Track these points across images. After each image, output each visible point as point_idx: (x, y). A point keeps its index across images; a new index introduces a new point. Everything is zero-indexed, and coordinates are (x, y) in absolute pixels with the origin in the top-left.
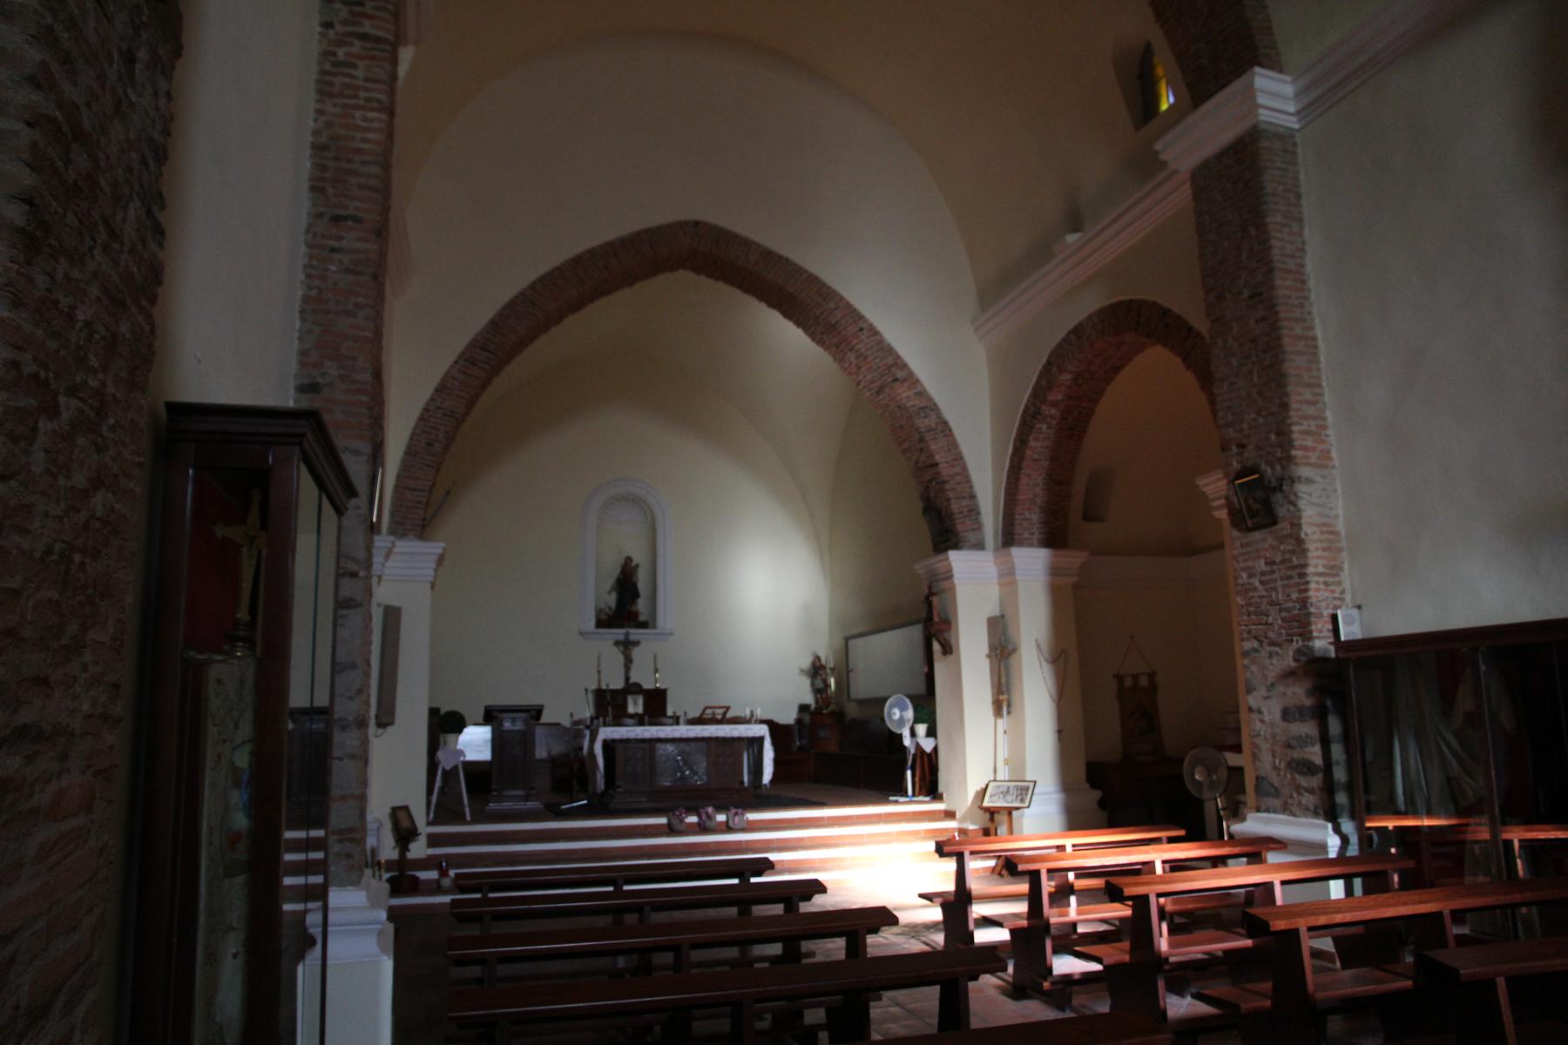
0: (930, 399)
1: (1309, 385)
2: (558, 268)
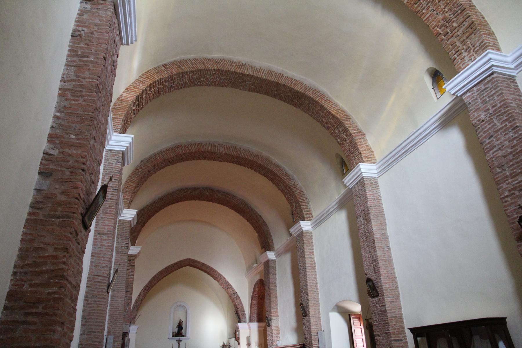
0: (235, 291)
1: (275, 303)
2: (162, 270)
